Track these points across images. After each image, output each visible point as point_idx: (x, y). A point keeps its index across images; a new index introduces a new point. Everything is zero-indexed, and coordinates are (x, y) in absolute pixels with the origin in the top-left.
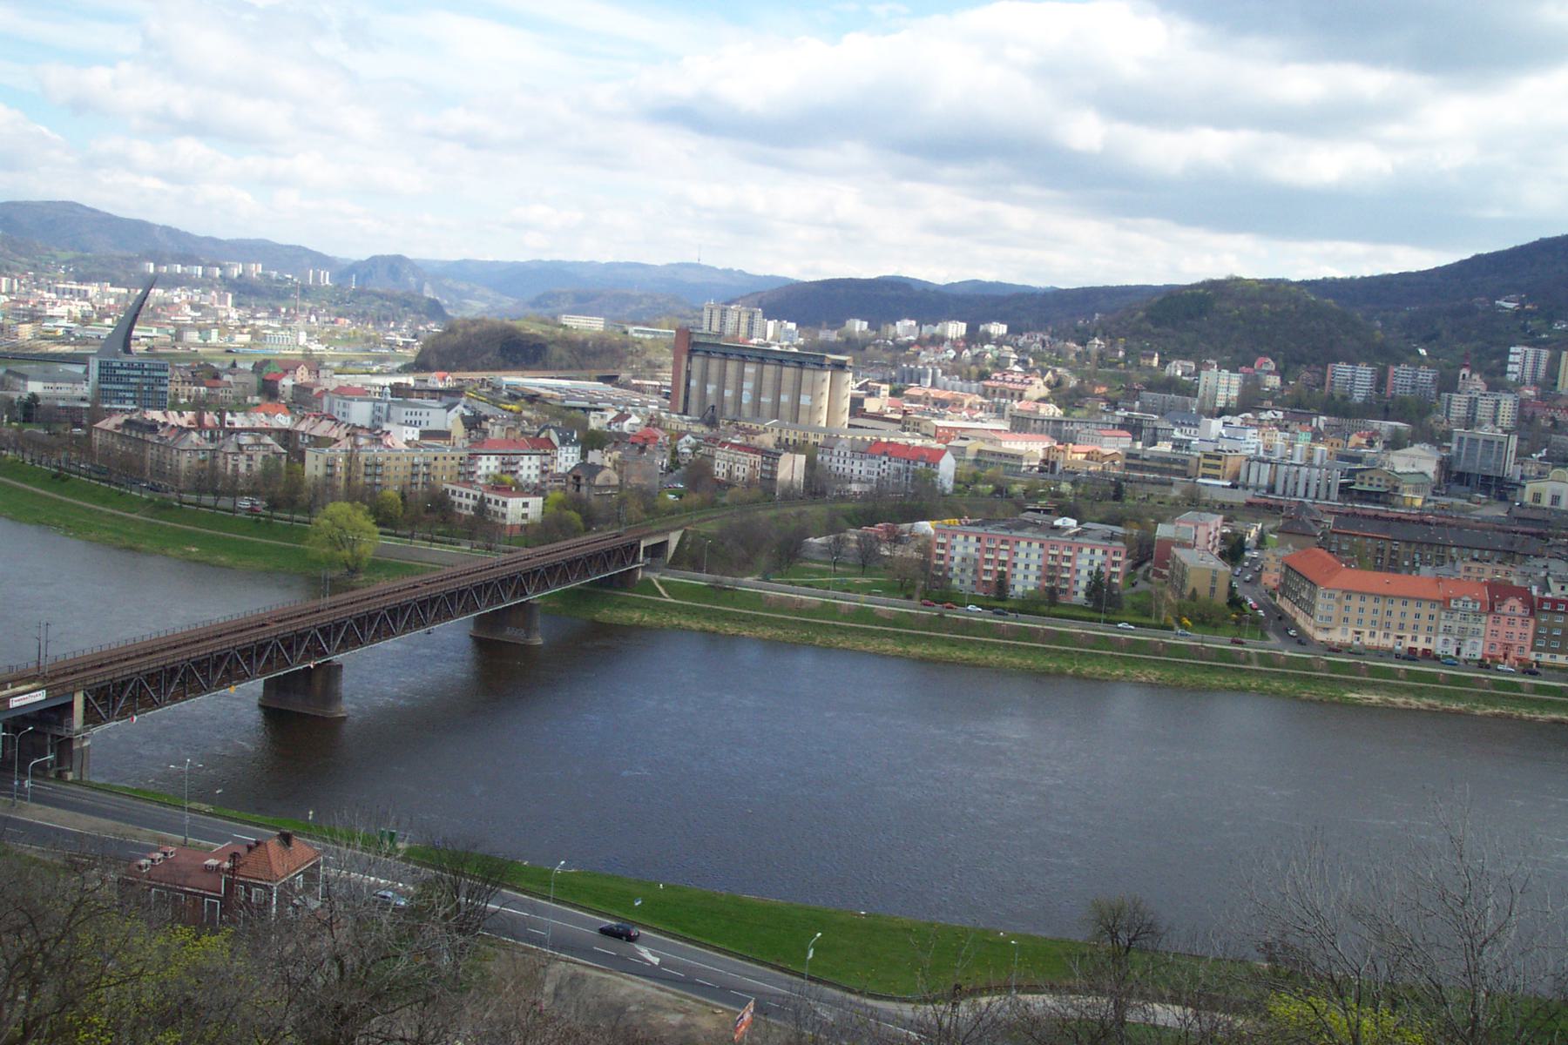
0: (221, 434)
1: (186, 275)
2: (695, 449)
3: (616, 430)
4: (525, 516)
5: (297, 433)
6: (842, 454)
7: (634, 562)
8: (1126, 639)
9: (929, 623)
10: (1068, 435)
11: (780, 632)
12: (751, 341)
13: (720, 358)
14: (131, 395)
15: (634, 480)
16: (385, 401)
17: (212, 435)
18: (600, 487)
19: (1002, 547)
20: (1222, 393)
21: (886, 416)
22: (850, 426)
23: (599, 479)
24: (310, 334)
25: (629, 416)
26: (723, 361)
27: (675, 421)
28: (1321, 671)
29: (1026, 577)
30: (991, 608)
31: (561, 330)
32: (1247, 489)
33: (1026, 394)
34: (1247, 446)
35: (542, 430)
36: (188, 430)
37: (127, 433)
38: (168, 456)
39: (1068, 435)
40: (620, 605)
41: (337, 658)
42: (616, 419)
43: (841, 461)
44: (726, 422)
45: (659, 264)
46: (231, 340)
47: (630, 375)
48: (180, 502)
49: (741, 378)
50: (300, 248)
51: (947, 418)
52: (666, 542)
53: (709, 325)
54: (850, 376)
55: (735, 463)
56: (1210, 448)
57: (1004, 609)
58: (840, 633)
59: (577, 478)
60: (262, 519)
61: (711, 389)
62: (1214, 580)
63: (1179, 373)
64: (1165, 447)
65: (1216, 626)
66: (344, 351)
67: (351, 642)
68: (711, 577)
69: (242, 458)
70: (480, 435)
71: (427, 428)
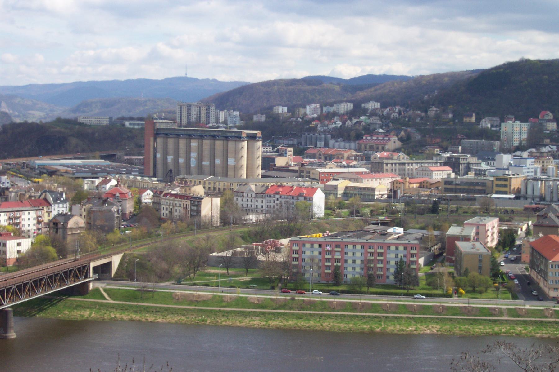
4: (19, 252)
6: (250, 195)
8: (417, 305)
9: (283, 305)
10: (410, 172)
11: (183, 318)
13: (175, 138)
19: (336, 249)
20: (516, 137)
21: (290, 168)
22: (263, 176)
25: (110, 180)
28: (550, 317)
29: (354, 268)
30: (328, 291)
31: (77, 126)
32: (526, 199)
33: (387, 147)
34: (529, 170)
39: (410, 172)
42: (101, 184)
43: (250, 200)
49: (189, 150)
51: (328, 166)
52: (109, 264)
54: (260, 143)
55: (173, 206)
56: (500, 174)
57: (338, 291)
58: (223, 316)
61: (170, 158)
62: (480, 261)
63: (489, 126)
64: (471, 175)
65: (481, 292)
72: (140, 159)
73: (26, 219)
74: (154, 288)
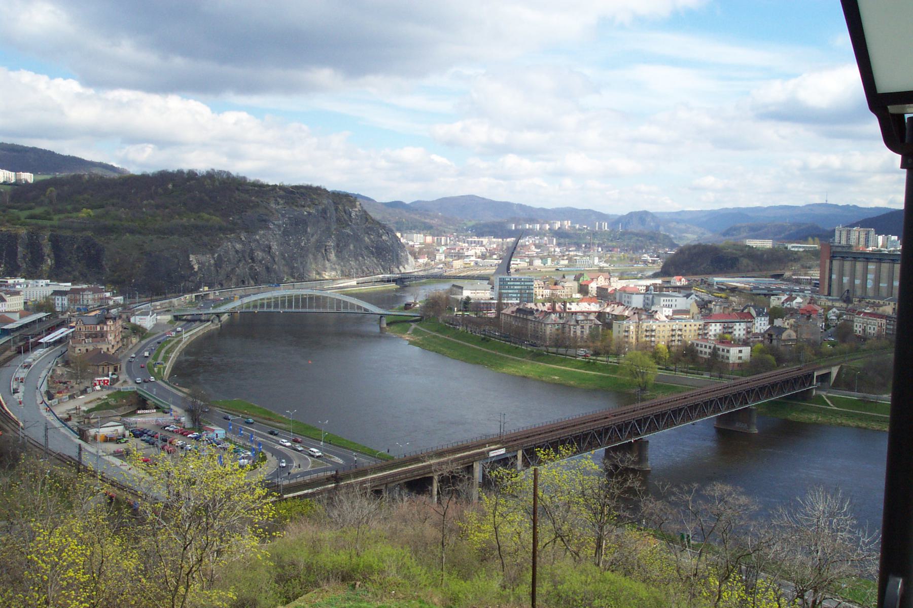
0: (565, 315)
1: (531, 229)
2: (839, 317)
3: (789, 306)
4: (740, 358)
5: (605, 313)
7: (810, 385)
12: (868, 249)
14: (515, 295)
15: (805, 336)
16: (651, 294)
17: (560, 315)
18: (784, 341)
23: (784, 336)
24: (600, 258)
25: (795, 298)
26: (853, 262)
27: (824, 301)
35: (745, 308)
36: (550, 313)
37: (518, 315)
38: (540, 327)
40: (803, 411)
41: (645, 437)
42: (787, 300)
44: (857, 299)
45: (801, 205)
46: (558, 263)
47: (791, 273)
48: (548, 352)
49: (866, 271)
50: (590, 210)
52: (829, 373)
53: (840, 239)
59: (770, 335)
60: (592, 361)
61: (846, 280)
66: (619, 266)
67: (653, 428)
68: (861, 394)
69: (578, 327)
70: (707, 311)
71: (676, 309)
72: (808, 279)
73: (737, 330)
74: (877, 400)
